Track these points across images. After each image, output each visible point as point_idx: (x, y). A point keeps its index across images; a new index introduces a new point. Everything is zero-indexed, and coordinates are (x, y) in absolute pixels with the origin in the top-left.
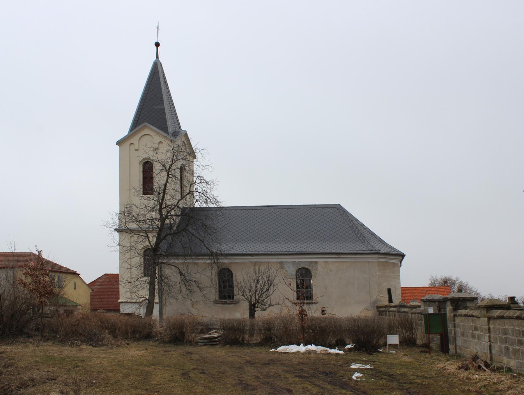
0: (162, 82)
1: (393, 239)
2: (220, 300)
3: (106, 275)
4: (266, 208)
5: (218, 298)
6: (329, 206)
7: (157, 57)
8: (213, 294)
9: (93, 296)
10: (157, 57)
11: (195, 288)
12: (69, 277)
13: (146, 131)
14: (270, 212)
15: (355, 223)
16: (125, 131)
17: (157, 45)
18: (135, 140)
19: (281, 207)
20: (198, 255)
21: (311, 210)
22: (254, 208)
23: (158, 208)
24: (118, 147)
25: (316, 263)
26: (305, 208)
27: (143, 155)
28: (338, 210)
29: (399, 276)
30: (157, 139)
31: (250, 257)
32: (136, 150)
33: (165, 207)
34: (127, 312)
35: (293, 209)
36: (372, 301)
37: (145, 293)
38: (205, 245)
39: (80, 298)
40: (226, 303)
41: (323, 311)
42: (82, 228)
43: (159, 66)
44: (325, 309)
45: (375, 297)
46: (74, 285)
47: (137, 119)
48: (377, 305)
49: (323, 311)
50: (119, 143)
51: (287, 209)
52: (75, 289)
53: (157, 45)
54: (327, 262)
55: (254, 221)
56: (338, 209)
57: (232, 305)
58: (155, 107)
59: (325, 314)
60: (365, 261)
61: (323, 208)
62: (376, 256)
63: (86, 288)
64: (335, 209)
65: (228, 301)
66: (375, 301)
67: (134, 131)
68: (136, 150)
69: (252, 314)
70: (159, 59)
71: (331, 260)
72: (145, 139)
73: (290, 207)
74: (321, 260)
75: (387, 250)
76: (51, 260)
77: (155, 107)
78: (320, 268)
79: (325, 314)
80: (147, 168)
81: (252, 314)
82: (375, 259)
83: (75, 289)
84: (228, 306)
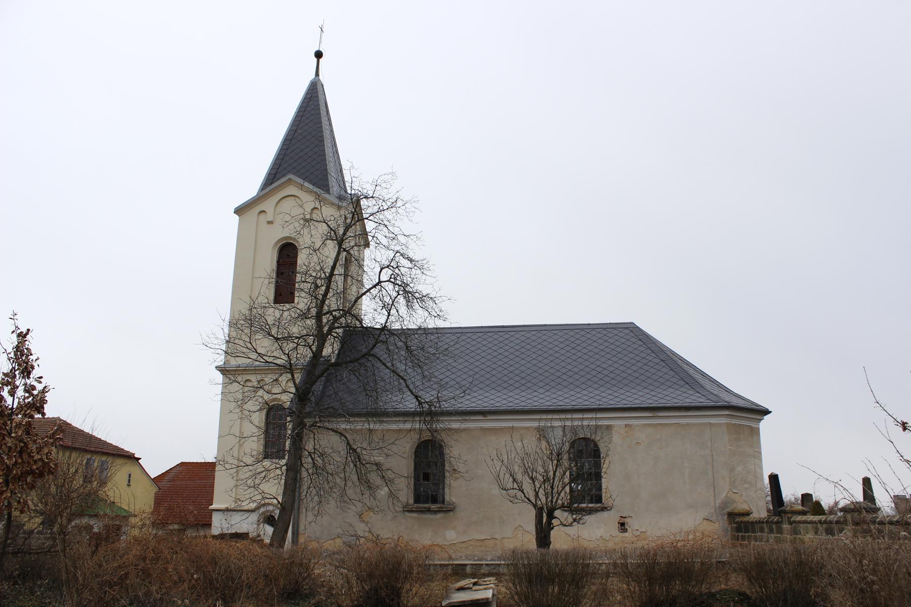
0: (323, 112)
1: (743, 385)
2: (416, 505)
3: (182, 464)
4: (499, 330)
5: (411, 501)
6: (614, 326)
7: (317, 74)
8: (406, 494)
9: (159, 500)
10: (317, 74)
11: (374, 478)
12: (120, 461)
13: (291, 190)
14: (507, 336)
15: (668, 353)
16: (252, 190)
17: (319, 55)
18: (268, 205)
19: (526, 329)
20: (385, 414)
21: (583, 333)
22: (475, 330)
23: (314, 311)
24: (237, 217)
25: (609, 427)
26: (572, 330)
27: (279, 233)
28: (631, 333)
29: (760, 453)
30: (308, 201)
31: (481, 418)
32: (270, 223)
33: (327, 313)
34: (233, 531)
35: (550, 331)
36: (718, 502)
37: (274, 489)
38: (408, 386)
39: (133, 498)
40: (429, 511)
41: (622, 524)
42: (152, 382)
43: (319, 87)
44: (626, 520)
45: (723, 495)
46: (131, 483)
47: (274, 172)
48: (728, 510)
49: (622, 524)
50: (239, 211)
51: (539, 331)
52: (129, 485)
53: (319, 55)
54: (630, 426)
55: (479, 351)
56: (631, 331)
57: (439, 516)
58: (306, 153)
59: (625, 531)
60: (704, 424)
61: (604, 329)
62: (727, 412)
63: (149, 483)
64: (627, 331)
65: (434, 507)
66: (725, 504)
67: (268, 190)
68: (270, 223)
69: (543, 538)
70: (321, 77)
71: (638, 421)
72: (288, 204)
73: (544, 328)
74: (618, 423)
75: (741, 403)
76: (87, 429)
77: (306, 153)
78: (616, 438)
79: (625, 531)
80: (287, 253)
81: (543, 538)
82: (720, 420)
83: (129, 485)
84: (432, 516)
